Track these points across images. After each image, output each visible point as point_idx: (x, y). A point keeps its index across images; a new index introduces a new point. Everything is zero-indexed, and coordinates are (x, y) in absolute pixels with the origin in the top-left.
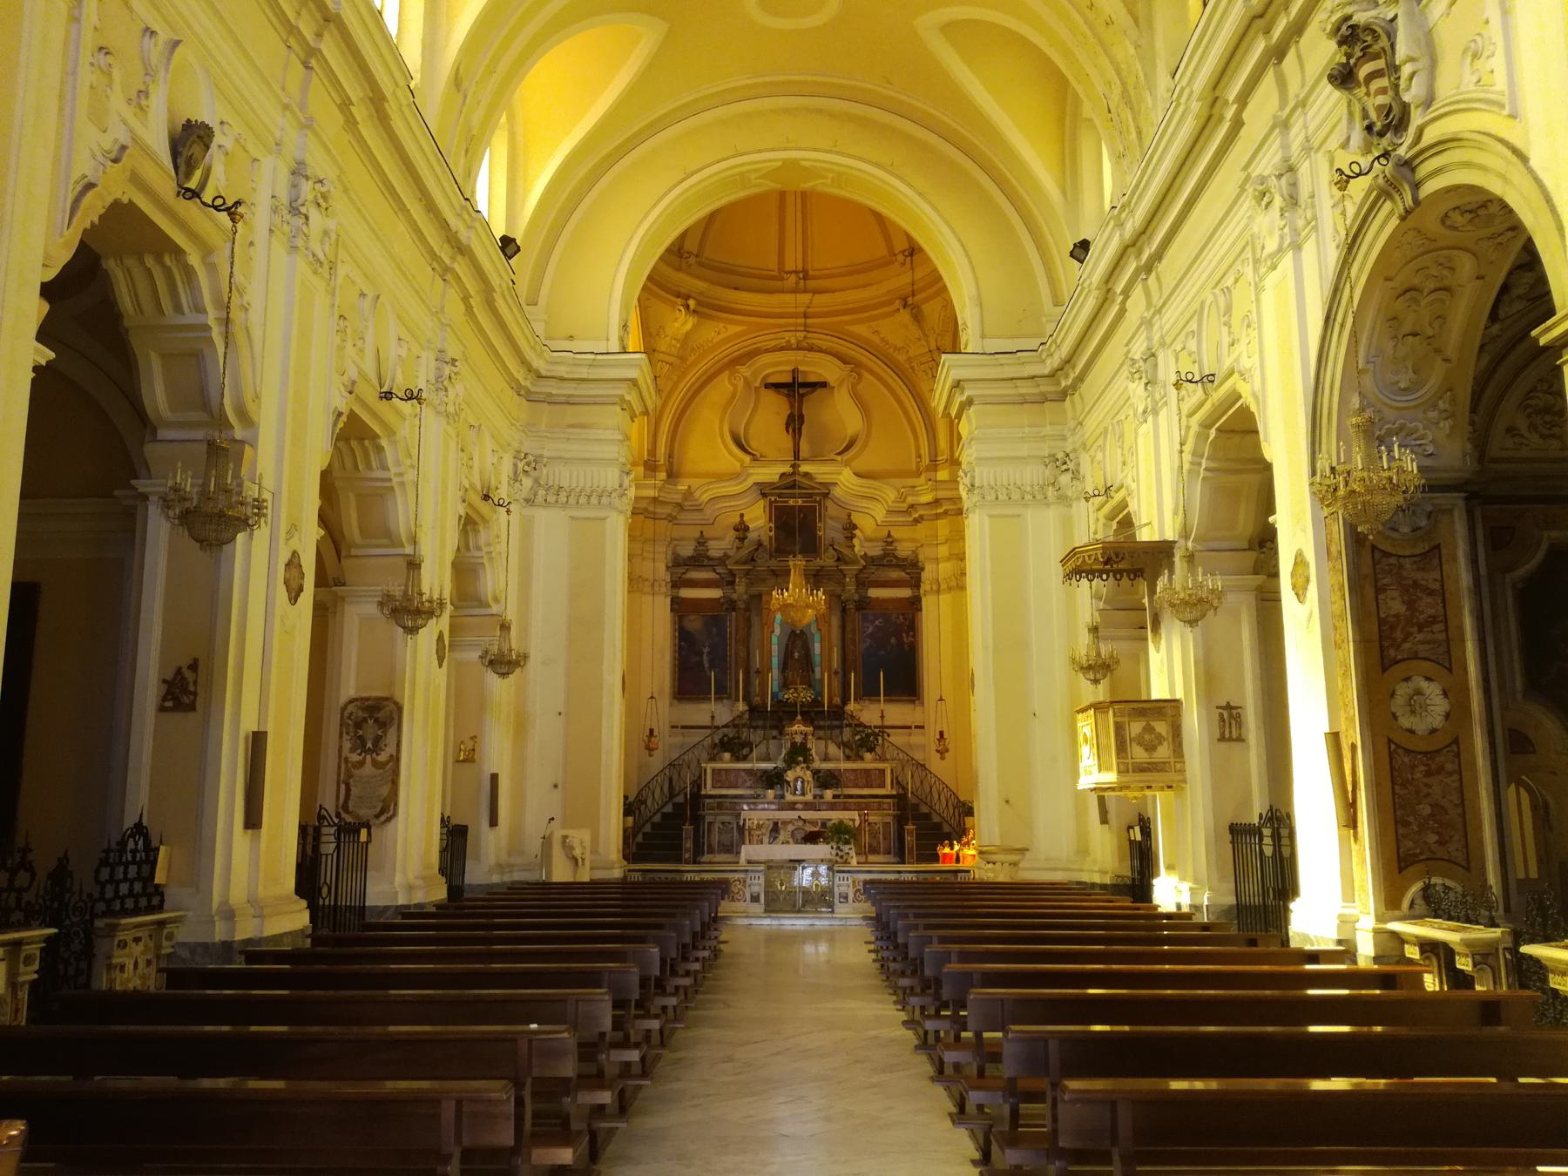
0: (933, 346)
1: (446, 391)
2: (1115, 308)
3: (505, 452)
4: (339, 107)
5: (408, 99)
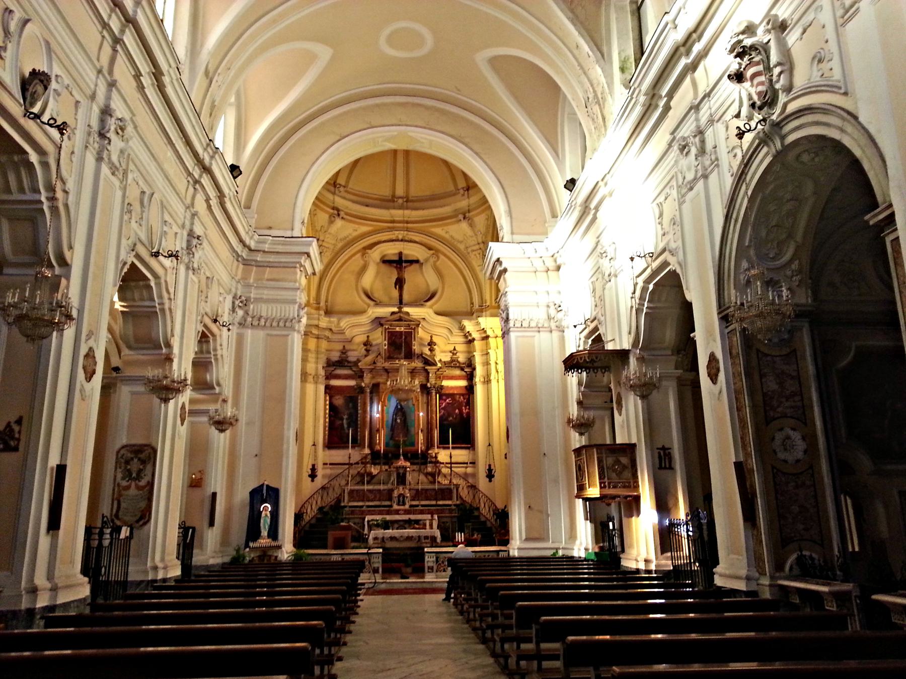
0: (480, 241)
1: (193, 254)
2: (590, 217)
3: (228, 294)
4: (134, 76)
5: (176, 76)
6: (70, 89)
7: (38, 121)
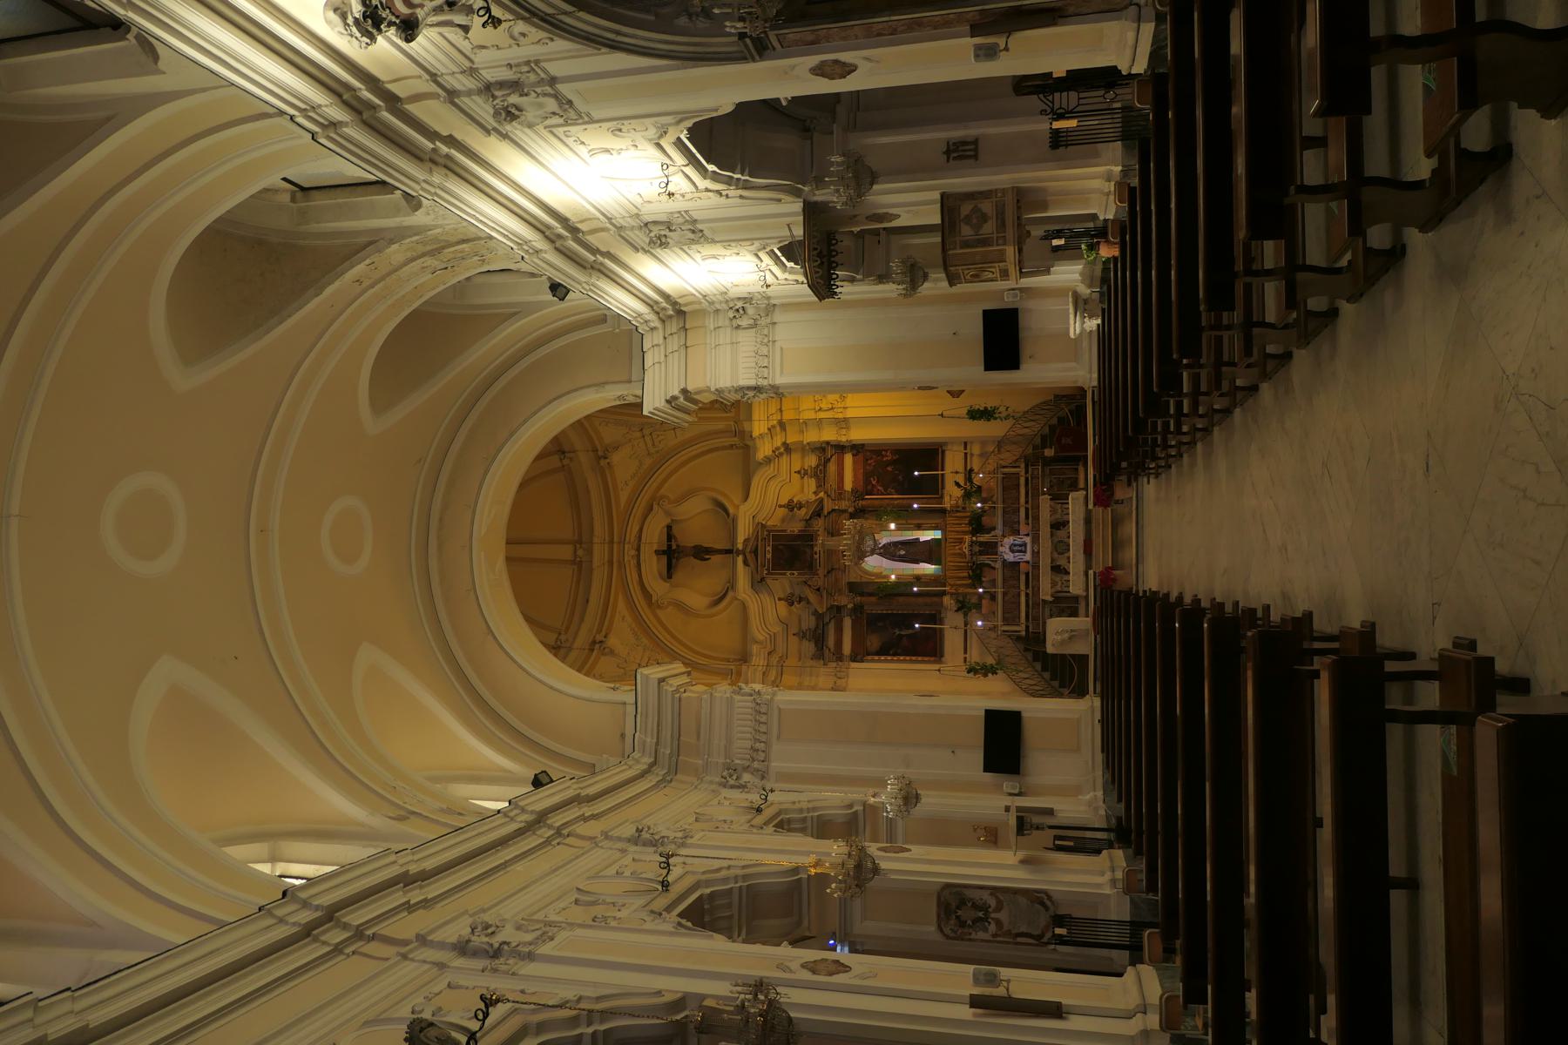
0: (638, 434)
1: (663, 837)
4: (409, 913)
5: (407, 854)
6: (430, 996)
7: (478, 1035)
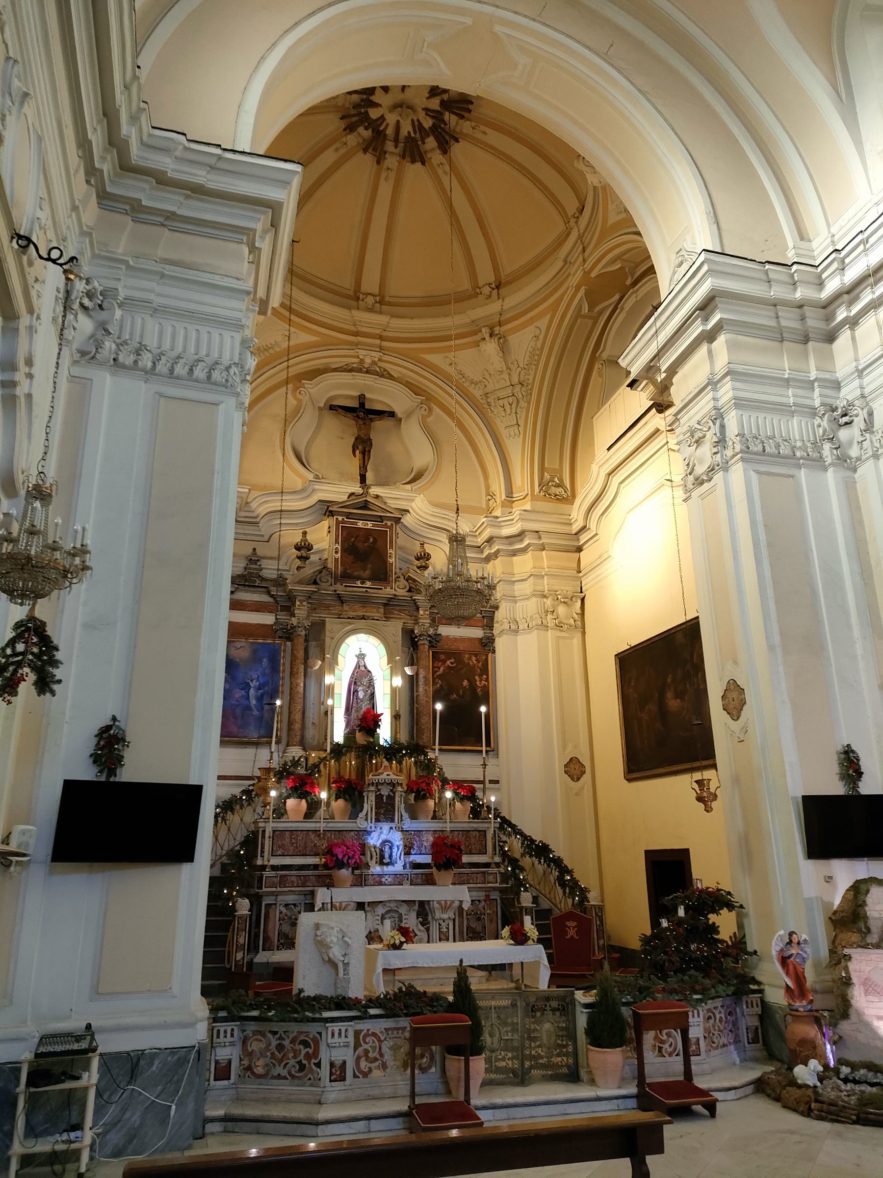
0: (515, 380)
